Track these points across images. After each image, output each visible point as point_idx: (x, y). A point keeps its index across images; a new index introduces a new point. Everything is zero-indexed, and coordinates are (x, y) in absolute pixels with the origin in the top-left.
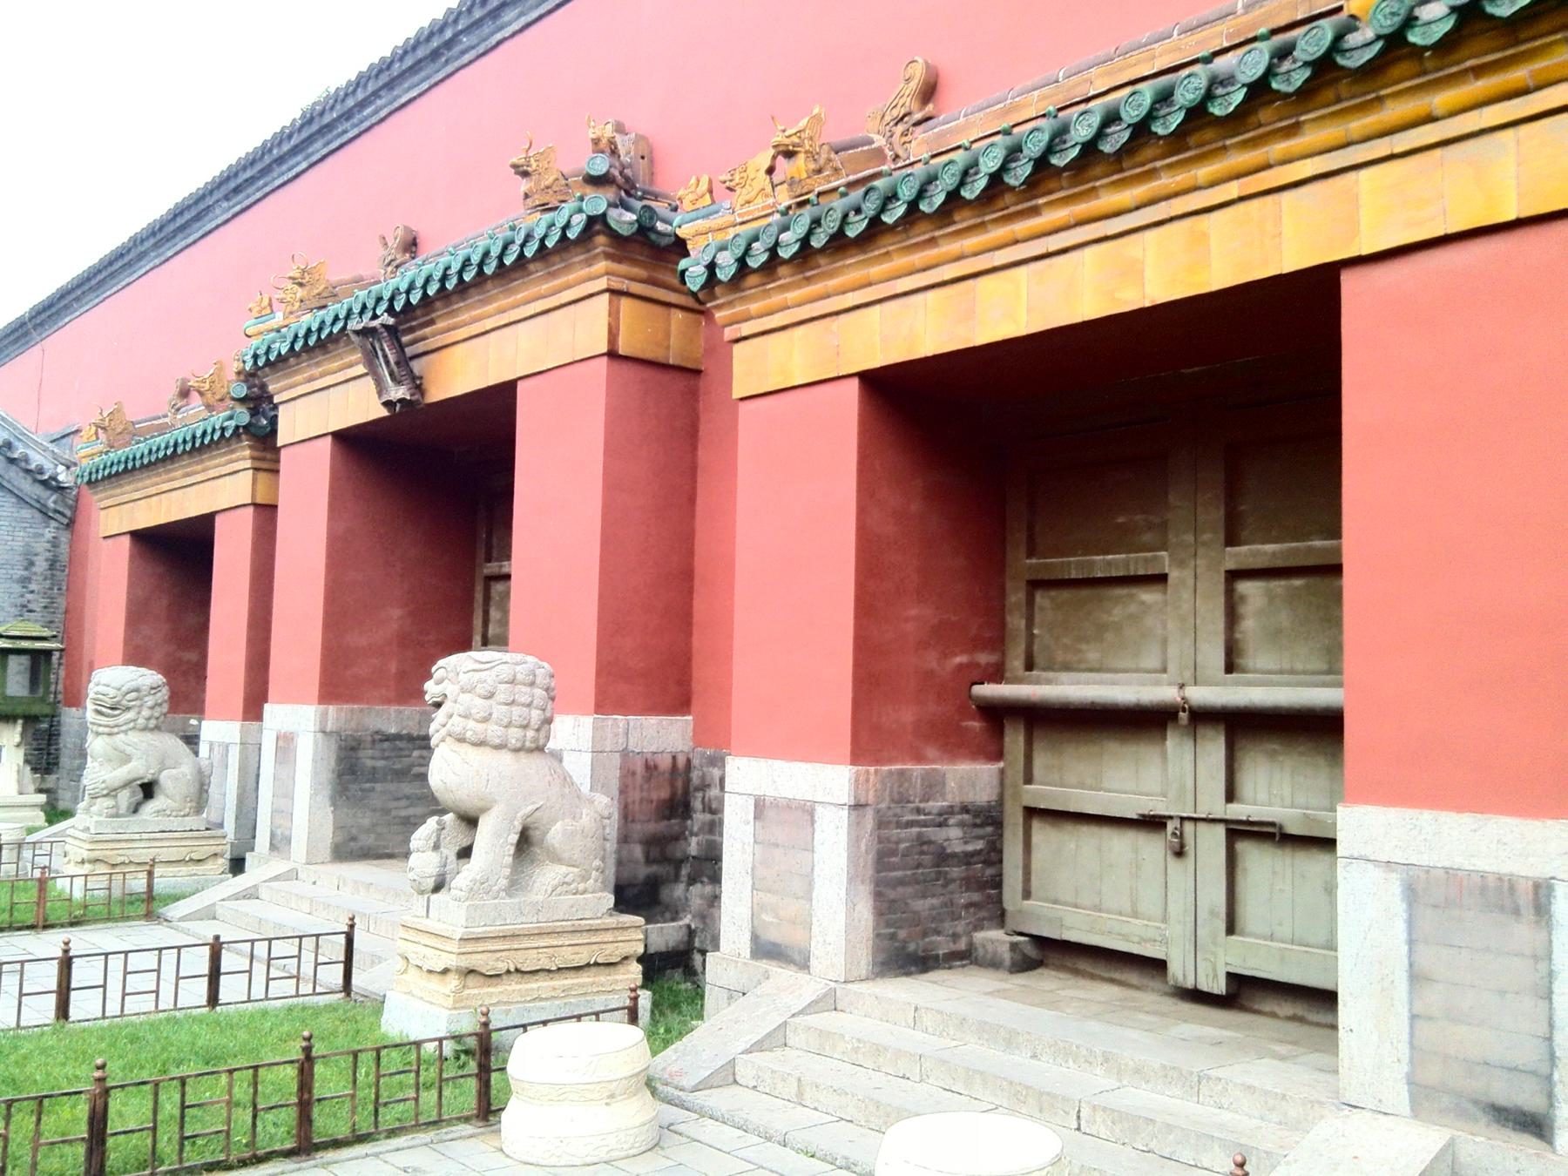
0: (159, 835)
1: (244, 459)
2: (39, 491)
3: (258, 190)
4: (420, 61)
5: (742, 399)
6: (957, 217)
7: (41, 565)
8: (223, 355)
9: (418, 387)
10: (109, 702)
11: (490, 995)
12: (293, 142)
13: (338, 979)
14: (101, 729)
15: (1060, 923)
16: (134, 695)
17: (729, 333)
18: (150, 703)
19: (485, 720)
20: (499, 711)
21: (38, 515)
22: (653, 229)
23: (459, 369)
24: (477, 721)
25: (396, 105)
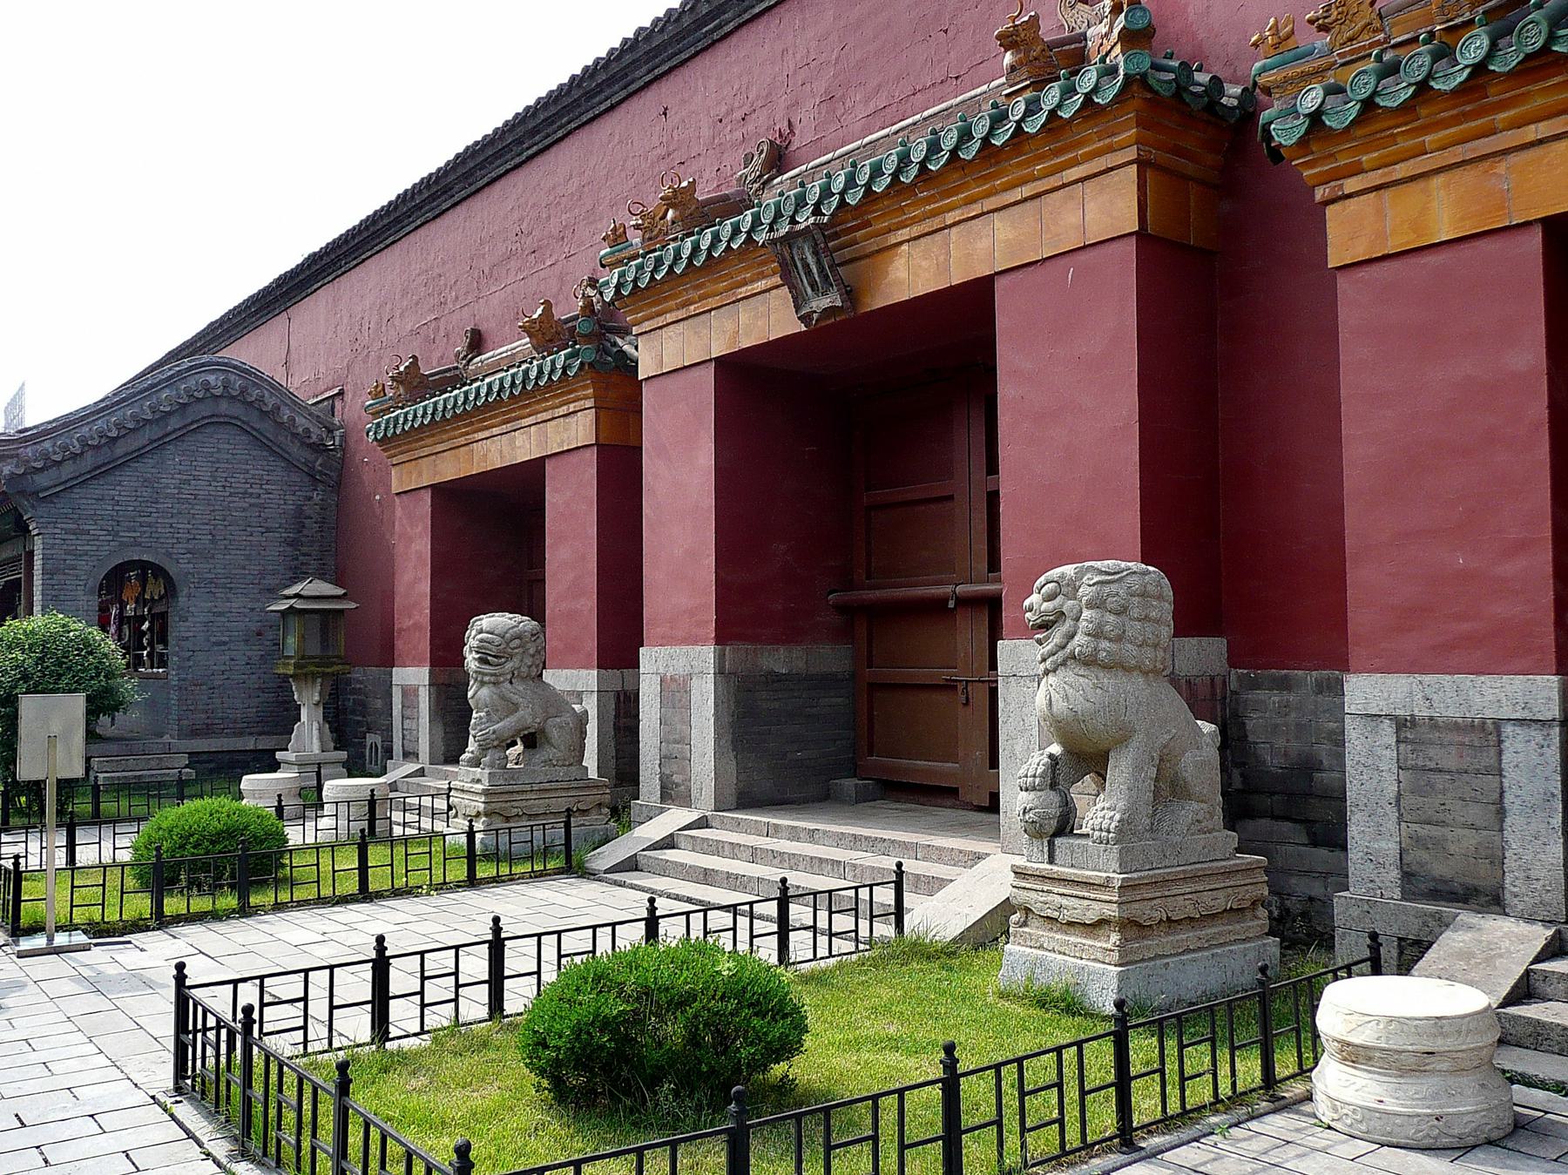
0: (547, 786)
1: (586, 398)
2: (308, 455)
3: (560, 128)
4: (638, 60)
5: (1338, 268)
6: (1492, 90)
7: (312, 527)
8: (570, 280)
9: (851, 294)
10: (494, 651)
11: (1148, 948)
12: (547, 114)
13: (793, 908)
14: (486, 679)
15: (1010, 738)
16: (517, 642)
17: (1320, 194)
18: (532, 651)
19: (1119, 639)
20: (1134, 629)
21: (306, 479)
22: (1186, 90)
23: (913, 270)
24: (1110, 640)
25: (746, 16)
